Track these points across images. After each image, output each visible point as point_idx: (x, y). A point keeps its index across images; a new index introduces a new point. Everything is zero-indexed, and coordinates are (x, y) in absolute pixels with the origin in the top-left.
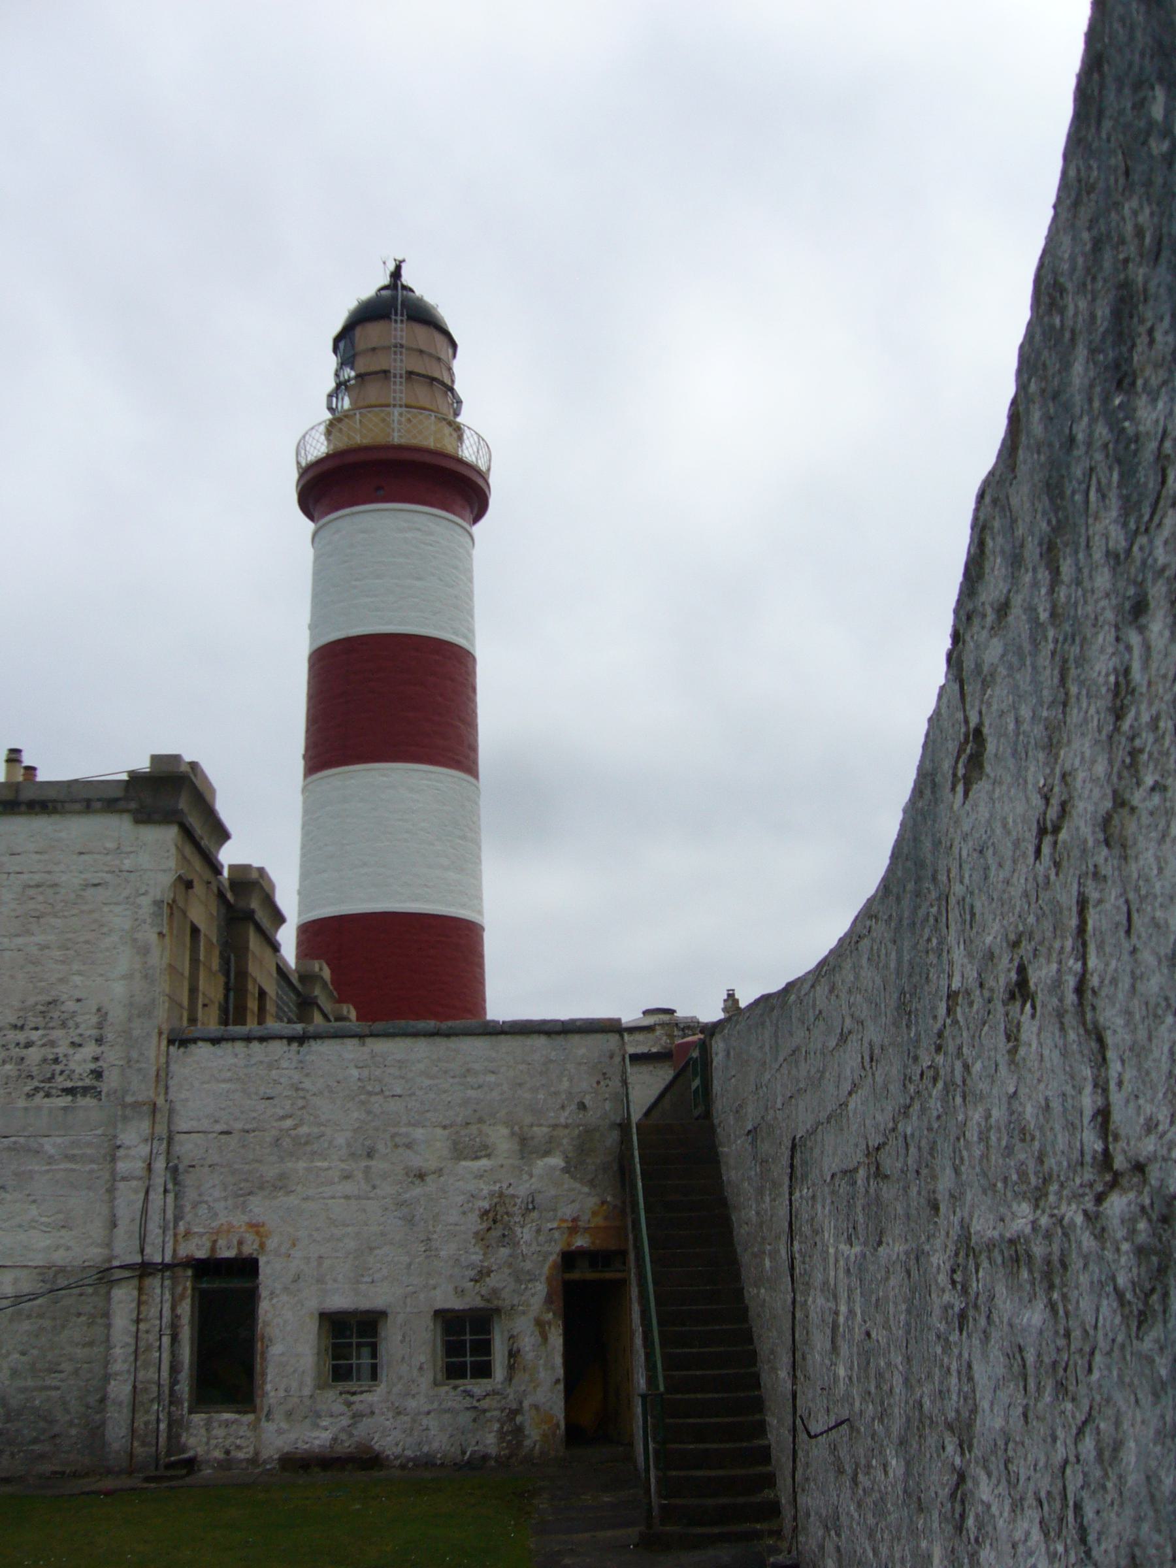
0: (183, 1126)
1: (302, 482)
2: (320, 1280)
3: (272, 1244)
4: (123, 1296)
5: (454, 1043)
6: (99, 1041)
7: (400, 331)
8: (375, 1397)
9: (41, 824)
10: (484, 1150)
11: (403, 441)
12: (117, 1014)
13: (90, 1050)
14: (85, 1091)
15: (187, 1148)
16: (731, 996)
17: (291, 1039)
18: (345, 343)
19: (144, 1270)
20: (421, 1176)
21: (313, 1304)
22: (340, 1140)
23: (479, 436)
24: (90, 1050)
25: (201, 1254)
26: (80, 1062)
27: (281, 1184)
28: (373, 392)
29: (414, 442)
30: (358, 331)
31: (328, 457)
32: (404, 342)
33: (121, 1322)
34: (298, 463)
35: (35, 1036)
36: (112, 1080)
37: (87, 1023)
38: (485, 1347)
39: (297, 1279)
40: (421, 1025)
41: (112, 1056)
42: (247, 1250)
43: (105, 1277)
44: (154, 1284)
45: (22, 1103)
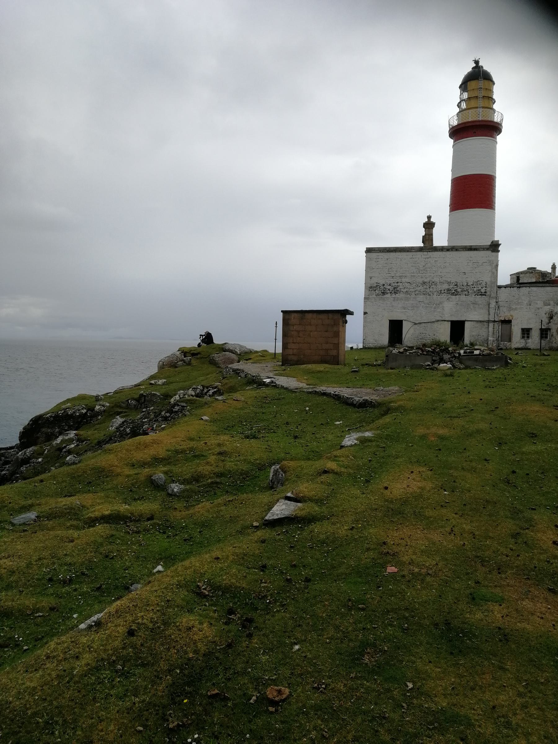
0: (499, 300)
1: (450, 131)
2: (522, 324)
3: (514, 318)
4: (491, 325)
5: (545, 288)
6: (486, 287)
7: (481, 83)
8: (530, 341)
9: (475, 252)
10: (549, 305)
11: (483, 119)
12: (488, 283)
13: (484, 288)
14: (484, 295)
15: (500, 303)
16: (351, 313)
17: (518, 287)
18: (464, 86)
19: (494, 321)
20: (538, 308)
21: (521, 327)
22: (525, 303)
23: (502, 114)
24: (484, 288)
25: (503, 319)
26: (483, 290)
27: (516, 309)
28: (473, 103)
29: (485, 119)
30: (469, 83)
31: (458, 125)
32: (482, 87)
33: (491, 329)
34: (449, 125)
35: (475, 286)
36: (488, 293)
37: (484, 284)
38: (547, 334)
39: (518, 323)
40: (554, 285)
41: (488, 289)
42: (510, 319)
43: (488, 322)
44: (496, 323)
45: (474, 296)
